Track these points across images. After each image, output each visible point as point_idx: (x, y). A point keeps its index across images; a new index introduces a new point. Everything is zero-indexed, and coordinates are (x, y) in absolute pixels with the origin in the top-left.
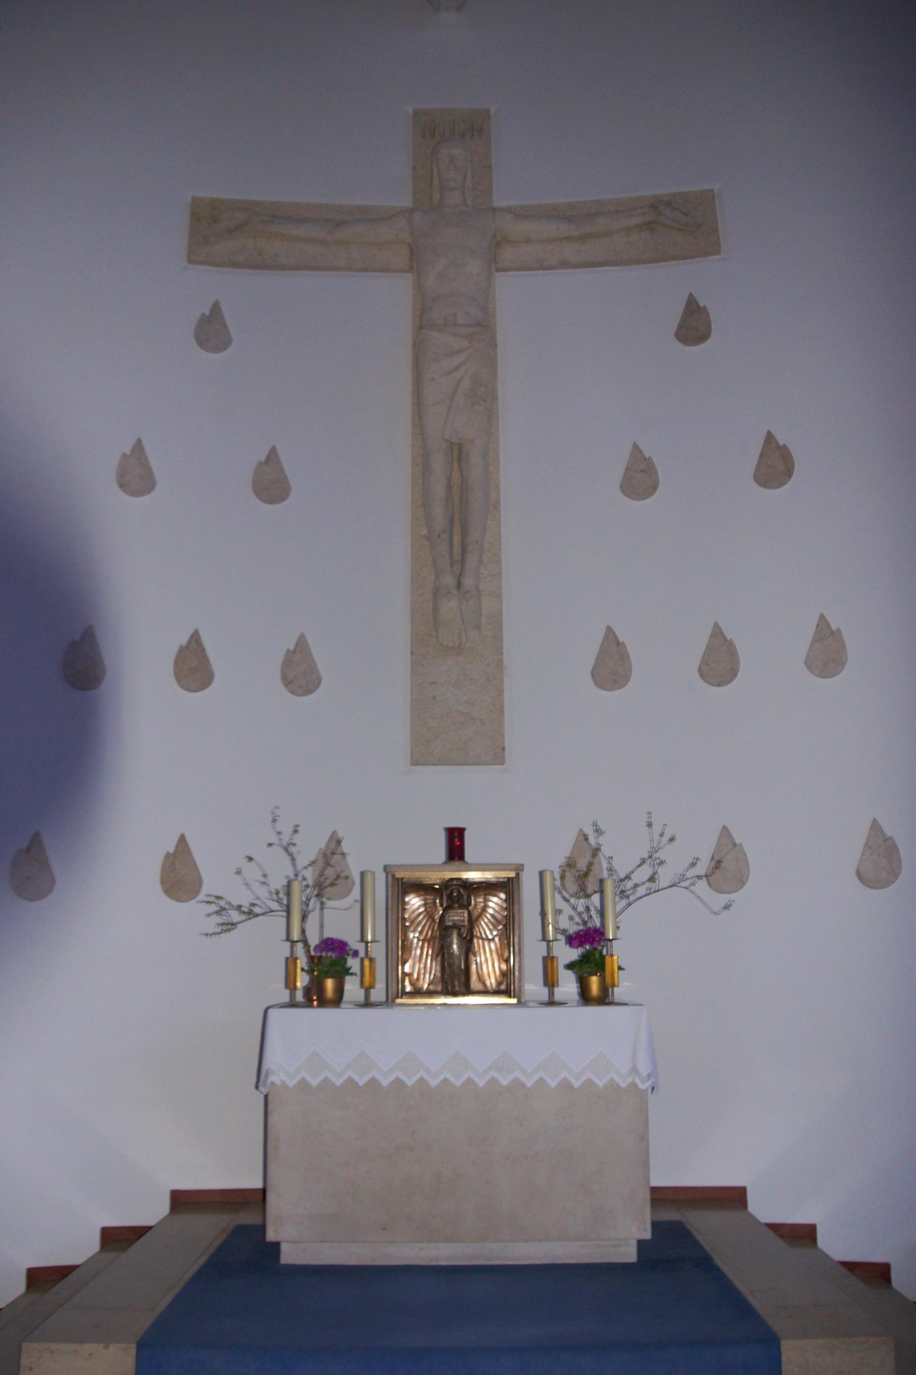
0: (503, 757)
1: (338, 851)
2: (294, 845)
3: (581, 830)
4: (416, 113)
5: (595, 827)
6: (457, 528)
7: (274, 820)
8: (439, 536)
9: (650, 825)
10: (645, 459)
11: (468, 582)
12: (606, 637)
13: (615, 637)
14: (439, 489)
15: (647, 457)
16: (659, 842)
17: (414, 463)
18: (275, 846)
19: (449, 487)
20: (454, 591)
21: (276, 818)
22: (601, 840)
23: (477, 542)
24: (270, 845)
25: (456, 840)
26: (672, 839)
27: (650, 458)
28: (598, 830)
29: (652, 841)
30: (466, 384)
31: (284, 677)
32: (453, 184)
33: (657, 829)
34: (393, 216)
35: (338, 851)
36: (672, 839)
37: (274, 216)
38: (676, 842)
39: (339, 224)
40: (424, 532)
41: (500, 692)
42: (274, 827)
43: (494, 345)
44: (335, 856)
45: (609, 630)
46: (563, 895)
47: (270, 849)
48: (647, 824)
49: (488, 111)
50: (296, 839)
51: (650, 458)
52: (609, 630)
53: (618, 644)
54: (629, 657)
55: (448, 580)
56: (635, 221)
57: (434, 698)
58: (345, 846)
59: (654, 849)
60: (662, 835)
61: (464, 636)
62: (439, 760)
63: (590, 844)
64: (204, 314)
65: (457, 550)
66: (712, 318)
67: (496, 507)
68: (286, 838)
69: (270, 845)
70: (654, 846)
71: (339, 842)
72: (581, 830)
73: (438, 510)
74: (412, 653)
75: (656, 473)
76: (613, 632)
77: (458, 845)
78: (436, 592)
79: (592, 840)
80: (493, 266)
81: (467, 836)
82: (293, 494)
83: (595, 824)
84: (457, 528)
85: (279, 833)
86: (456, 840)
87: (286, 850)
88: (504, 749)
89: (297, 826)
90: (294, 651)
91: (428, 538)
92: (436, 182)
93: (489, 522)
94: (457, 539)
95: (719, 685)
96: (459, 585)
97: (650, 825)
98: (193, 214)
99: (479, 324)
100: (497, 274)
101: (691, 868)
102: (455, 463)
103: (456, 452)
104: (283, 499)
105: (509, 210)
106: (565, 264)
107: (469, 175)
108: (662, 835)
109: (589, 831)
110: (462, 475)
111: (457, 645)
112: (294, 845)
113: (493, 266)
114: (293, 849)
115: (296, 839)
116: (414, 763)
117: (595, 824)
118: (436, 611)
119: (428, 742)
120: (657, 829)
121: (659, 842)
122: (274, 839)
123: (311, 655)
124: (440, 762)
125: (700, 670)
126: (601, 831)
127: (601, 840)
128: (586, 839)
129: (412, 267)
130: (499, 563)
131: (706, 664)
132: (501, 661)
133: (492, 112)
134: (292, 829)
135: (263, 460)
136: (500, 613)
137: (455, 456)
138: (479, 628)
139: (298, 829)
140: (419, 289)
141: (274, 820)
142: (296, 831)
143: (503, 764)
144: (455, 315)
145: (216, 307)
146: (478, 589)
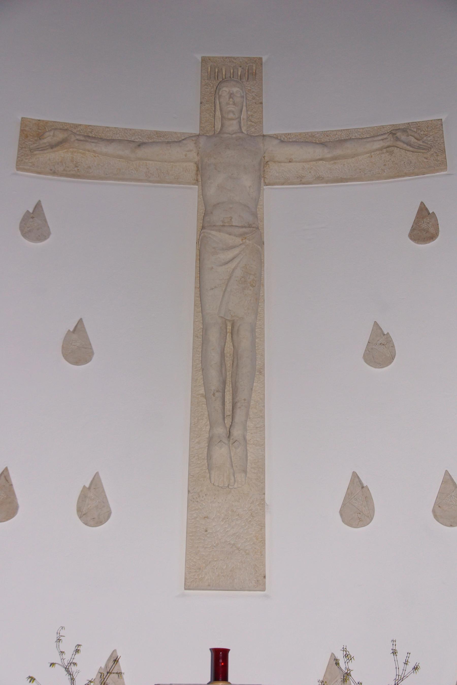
0: (264, 584)
1: (115, 671)
2: (75, 664)
3: (333, 654)
4: (204, 60)
5: (345, 653)
6: (229, 388)
7: (59, 640)
8: (214, 395)
9: (394, 652)
10: (384, 335)
11: (237, 432)
12: (352, 481)
13: (360, 481)
14: (214, 357)
15: (385, 333)
16: (404, 670)
17: (195, 336)
18: (56, 665)
19: (223, 355)
20: (226, 441)
21: (61, 638)
22: (351, 665)
23: (245, 400)
24: (52, 664)
25: (221, 661)
26: (416, 668)
27: (388, 333)
28: (348, 655)
29: (397, 668)
30: (238, 273)
31: (79, 510)
32: (231, 116)
33: (401, 657)
34: (183, 140)
35: (115, 671)
36: (416, 668)
37: (89, 137)
38: (419, 672)
39: (140, 145)
40: (202, 391)
41: (262, 526)
42: (58, 647)
43: (262, 243)
44: (112, 675)
45: (355, 476)
46: (205, 135)
47: (52, 669)
48: (392, 651)
49: (261, 59)
50: (77, 658)
51: (388, 333)
52: (355, 476)
53: (363, 487)
54: (86, 364)
55: (220, 431)
56: (377, 145)
57: (206, 531)
58: (123, 665)
59: (400, 677)
60: (406, 663)
61: (232, 478)
62: (209, 585)
63: (340, 668)
64: (28, 211)
65: (228, 406)
66: (439, 222)
67: (261, 372)
68: (67, 657)
69: (52, 664)
70: (400, 674)
71: (116, 661)
72: (333, 654)
73: (214, 374)
74: (189, 491)
75: (393, 346)
76: (358, 477)
77: (222, 666)
78: (210, 440)
79: (342, 665)
80: (262, 181)
81: (231, 656)
82: (95, 358)
83: (344, 650)
84: (229, 388)
85: (62, 653)
86: (221, 661)
87: (67, 669)
88: (265, 577)
89: (79, 645)
90: (89, 488)
91: (205, 397)
92: (218, 113)
93: (255, 384)
94: (228, 397)
95: (451, 526)
96: (229, 435)
97: (394, 652)
98: (22, 131)
99: (250, 226)
100: (265, 187)
101: (414, 667)
102: (229, 335)
103: (229, 327)
104: (86, 361)
105: (275, 137)
106: (320, 179)
107: (244, 108)
108: (406, 663)
109: (340, 656)
110: (234, 346)
111: (226, 485)
112: (75, 664)
113: (262, 181)
114: (73, 669)
115: (77, 658)
116: (187, 588)
117: (344, 650)
118: (209, 457)
119: (200, 569)
120: (401, 657)
121: (404, 670)
122: (57, 659)
123: (103, 491)
124: (209, 587)
125: (434, 511)
126: (351, 656)
127: (351, 665)
128: (337, 664)
129: (197, 180)
130: (263, 417)
131: (439, 507)
132: (264, 500)
133: (264, 60)
134: (73, 649)
135: (72, 330)
136: (264, 459)
137: (228, 330)
138: (245, 471)
139: (81, 648)
140: (203, 195)
141: (59, 640)
142: (77, 651)
143: (264, 590)
144: (231, 218)
145: (38, 206)
146: (245, 439)
